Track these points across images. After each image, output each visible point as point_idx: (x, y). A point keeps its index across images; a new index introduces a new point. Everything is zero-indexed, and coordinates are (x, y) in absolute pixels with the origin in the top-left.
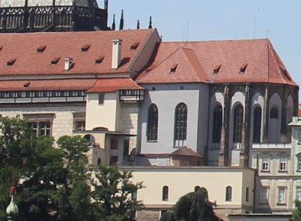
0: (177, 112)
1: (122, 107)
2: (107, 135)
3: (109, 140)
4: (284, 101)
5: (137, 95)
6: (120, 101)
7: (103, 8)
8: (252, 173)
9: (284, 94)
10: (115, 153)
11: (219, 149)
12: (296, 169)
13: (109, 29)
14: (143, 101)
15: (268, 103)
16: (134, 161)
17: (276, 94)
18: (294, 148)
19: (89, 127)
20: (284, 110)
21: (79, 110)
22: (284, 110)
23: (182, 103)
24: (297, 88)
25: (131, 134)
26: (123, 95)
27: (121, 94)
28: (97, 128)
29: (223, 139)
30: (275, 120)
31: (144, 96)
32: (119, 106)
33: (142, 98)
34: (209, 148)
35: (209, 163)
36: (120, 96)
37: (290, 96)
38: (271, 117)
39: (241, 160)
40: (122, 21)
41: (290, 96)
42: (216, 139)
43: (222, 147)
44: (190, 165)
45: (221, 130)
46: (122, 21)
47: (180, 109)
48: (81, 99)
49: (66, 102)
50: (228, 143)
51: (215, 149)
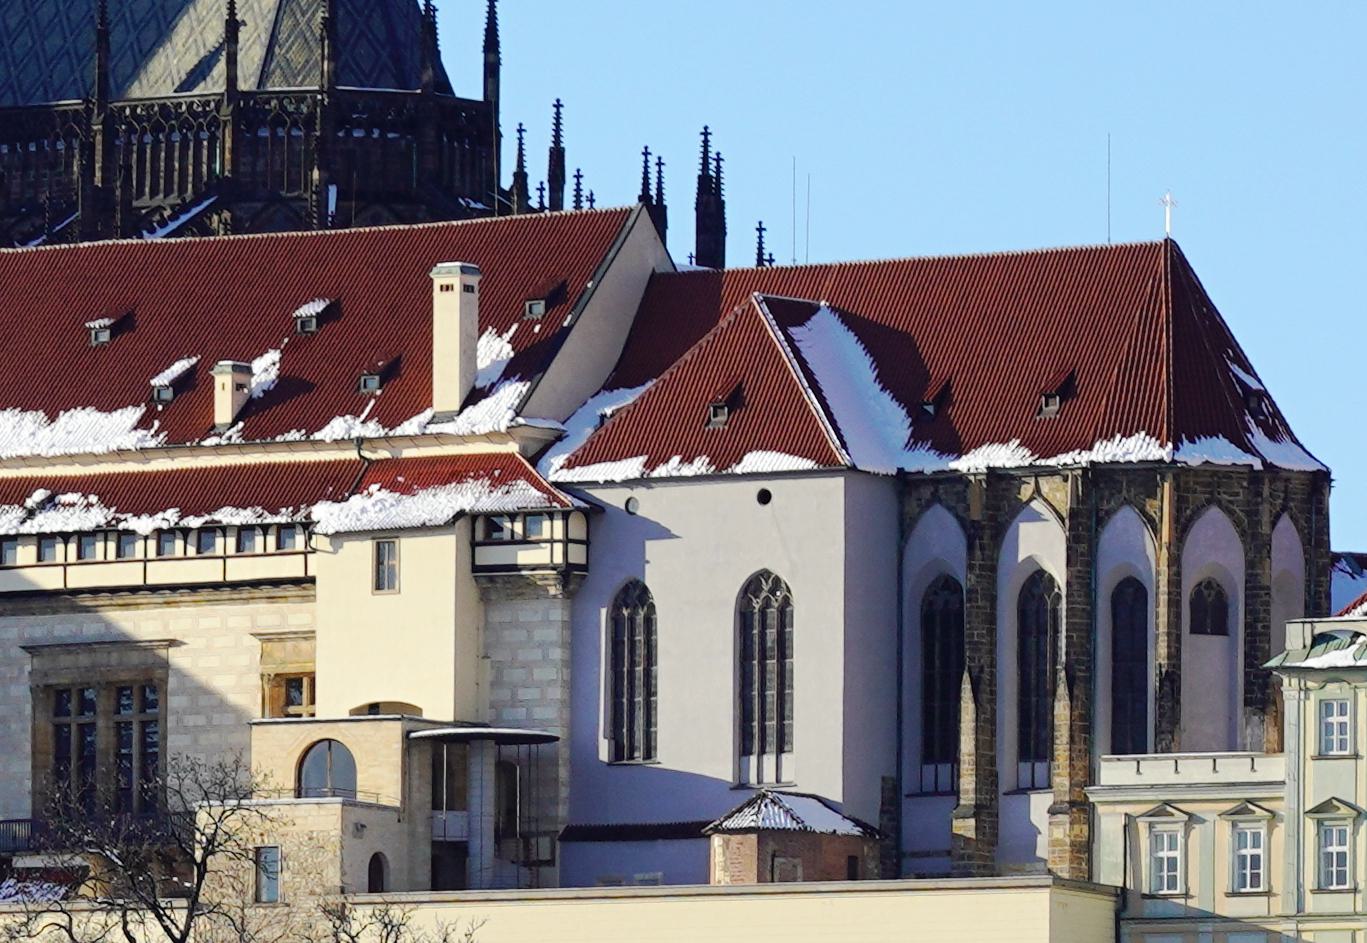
0: (744, 618)
1: (485, 598)
2: (409, 743)
3: (422, 760)
4: (1257, 547)
5: (552, 541)
6: (475, 569)
7: (479, 96)
8: (1105, 907)
9: (1253, 514)
10: (452, 825)
11: (955, 792)
12: (1310, 882)
13: (532, 210)
14: (584, 568)
15: (1175, 561)
16: (551, 863)
17: (1214, 513)
18: (1299, 776)
19: (333, 699)
20: (1256, 590)
21: (287, 615)
22: (1256, 590)
23: (765, 574)
24: (1320, 480)
25: (19, 563)
26: (489, 542)
27: (480, 536)
28: (374, 708)
29: (967, 744)
30: (1217, 641)
31: (587, 543)
32: (472, 592)
33: (578, 555)
34: (907, 786)
35: (906, 863)
36: (474, 544)
37: (1285, 521)
38: (1197, 629)
39: (656, 726)
40: (557, 156)
41: (1285, 521)
42: (941, 745)
43: (968, 782)
44: (807, 878)
45: (958, 699)
46: (557, 156)
47: (757, 605)
48: (291, 567)
49: (215, 586)
50: (992, 761)
51: (936, 793)
